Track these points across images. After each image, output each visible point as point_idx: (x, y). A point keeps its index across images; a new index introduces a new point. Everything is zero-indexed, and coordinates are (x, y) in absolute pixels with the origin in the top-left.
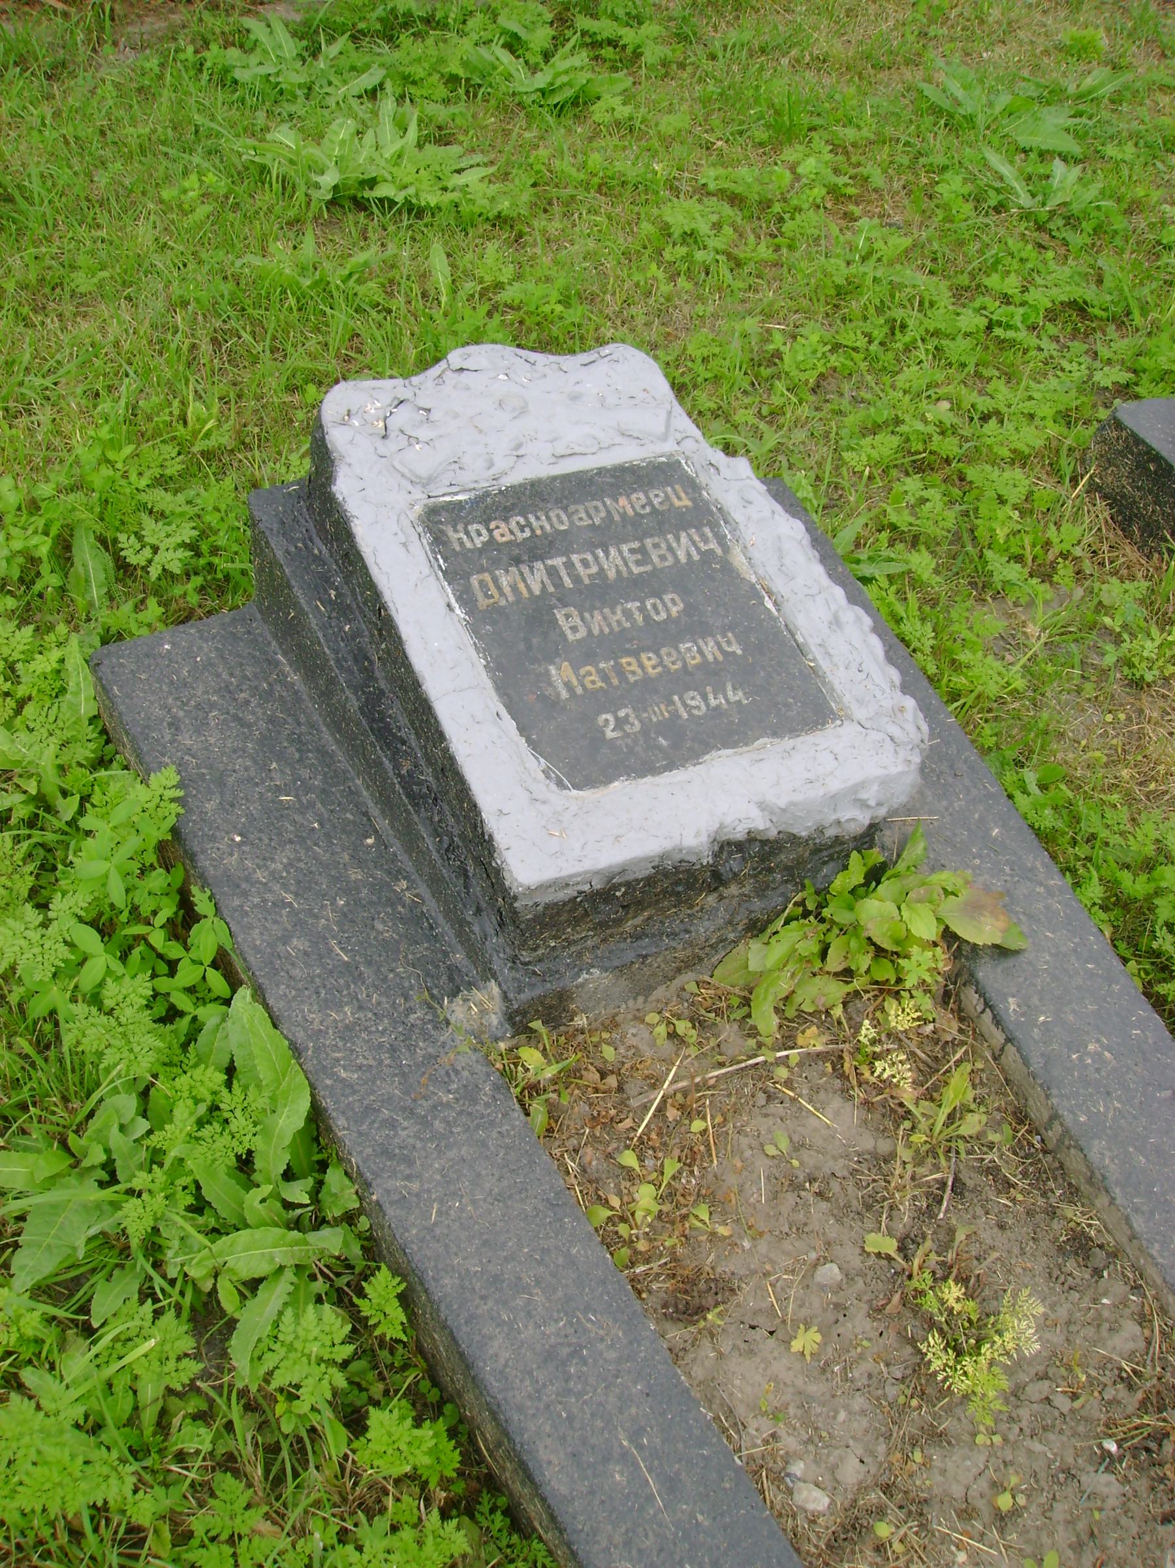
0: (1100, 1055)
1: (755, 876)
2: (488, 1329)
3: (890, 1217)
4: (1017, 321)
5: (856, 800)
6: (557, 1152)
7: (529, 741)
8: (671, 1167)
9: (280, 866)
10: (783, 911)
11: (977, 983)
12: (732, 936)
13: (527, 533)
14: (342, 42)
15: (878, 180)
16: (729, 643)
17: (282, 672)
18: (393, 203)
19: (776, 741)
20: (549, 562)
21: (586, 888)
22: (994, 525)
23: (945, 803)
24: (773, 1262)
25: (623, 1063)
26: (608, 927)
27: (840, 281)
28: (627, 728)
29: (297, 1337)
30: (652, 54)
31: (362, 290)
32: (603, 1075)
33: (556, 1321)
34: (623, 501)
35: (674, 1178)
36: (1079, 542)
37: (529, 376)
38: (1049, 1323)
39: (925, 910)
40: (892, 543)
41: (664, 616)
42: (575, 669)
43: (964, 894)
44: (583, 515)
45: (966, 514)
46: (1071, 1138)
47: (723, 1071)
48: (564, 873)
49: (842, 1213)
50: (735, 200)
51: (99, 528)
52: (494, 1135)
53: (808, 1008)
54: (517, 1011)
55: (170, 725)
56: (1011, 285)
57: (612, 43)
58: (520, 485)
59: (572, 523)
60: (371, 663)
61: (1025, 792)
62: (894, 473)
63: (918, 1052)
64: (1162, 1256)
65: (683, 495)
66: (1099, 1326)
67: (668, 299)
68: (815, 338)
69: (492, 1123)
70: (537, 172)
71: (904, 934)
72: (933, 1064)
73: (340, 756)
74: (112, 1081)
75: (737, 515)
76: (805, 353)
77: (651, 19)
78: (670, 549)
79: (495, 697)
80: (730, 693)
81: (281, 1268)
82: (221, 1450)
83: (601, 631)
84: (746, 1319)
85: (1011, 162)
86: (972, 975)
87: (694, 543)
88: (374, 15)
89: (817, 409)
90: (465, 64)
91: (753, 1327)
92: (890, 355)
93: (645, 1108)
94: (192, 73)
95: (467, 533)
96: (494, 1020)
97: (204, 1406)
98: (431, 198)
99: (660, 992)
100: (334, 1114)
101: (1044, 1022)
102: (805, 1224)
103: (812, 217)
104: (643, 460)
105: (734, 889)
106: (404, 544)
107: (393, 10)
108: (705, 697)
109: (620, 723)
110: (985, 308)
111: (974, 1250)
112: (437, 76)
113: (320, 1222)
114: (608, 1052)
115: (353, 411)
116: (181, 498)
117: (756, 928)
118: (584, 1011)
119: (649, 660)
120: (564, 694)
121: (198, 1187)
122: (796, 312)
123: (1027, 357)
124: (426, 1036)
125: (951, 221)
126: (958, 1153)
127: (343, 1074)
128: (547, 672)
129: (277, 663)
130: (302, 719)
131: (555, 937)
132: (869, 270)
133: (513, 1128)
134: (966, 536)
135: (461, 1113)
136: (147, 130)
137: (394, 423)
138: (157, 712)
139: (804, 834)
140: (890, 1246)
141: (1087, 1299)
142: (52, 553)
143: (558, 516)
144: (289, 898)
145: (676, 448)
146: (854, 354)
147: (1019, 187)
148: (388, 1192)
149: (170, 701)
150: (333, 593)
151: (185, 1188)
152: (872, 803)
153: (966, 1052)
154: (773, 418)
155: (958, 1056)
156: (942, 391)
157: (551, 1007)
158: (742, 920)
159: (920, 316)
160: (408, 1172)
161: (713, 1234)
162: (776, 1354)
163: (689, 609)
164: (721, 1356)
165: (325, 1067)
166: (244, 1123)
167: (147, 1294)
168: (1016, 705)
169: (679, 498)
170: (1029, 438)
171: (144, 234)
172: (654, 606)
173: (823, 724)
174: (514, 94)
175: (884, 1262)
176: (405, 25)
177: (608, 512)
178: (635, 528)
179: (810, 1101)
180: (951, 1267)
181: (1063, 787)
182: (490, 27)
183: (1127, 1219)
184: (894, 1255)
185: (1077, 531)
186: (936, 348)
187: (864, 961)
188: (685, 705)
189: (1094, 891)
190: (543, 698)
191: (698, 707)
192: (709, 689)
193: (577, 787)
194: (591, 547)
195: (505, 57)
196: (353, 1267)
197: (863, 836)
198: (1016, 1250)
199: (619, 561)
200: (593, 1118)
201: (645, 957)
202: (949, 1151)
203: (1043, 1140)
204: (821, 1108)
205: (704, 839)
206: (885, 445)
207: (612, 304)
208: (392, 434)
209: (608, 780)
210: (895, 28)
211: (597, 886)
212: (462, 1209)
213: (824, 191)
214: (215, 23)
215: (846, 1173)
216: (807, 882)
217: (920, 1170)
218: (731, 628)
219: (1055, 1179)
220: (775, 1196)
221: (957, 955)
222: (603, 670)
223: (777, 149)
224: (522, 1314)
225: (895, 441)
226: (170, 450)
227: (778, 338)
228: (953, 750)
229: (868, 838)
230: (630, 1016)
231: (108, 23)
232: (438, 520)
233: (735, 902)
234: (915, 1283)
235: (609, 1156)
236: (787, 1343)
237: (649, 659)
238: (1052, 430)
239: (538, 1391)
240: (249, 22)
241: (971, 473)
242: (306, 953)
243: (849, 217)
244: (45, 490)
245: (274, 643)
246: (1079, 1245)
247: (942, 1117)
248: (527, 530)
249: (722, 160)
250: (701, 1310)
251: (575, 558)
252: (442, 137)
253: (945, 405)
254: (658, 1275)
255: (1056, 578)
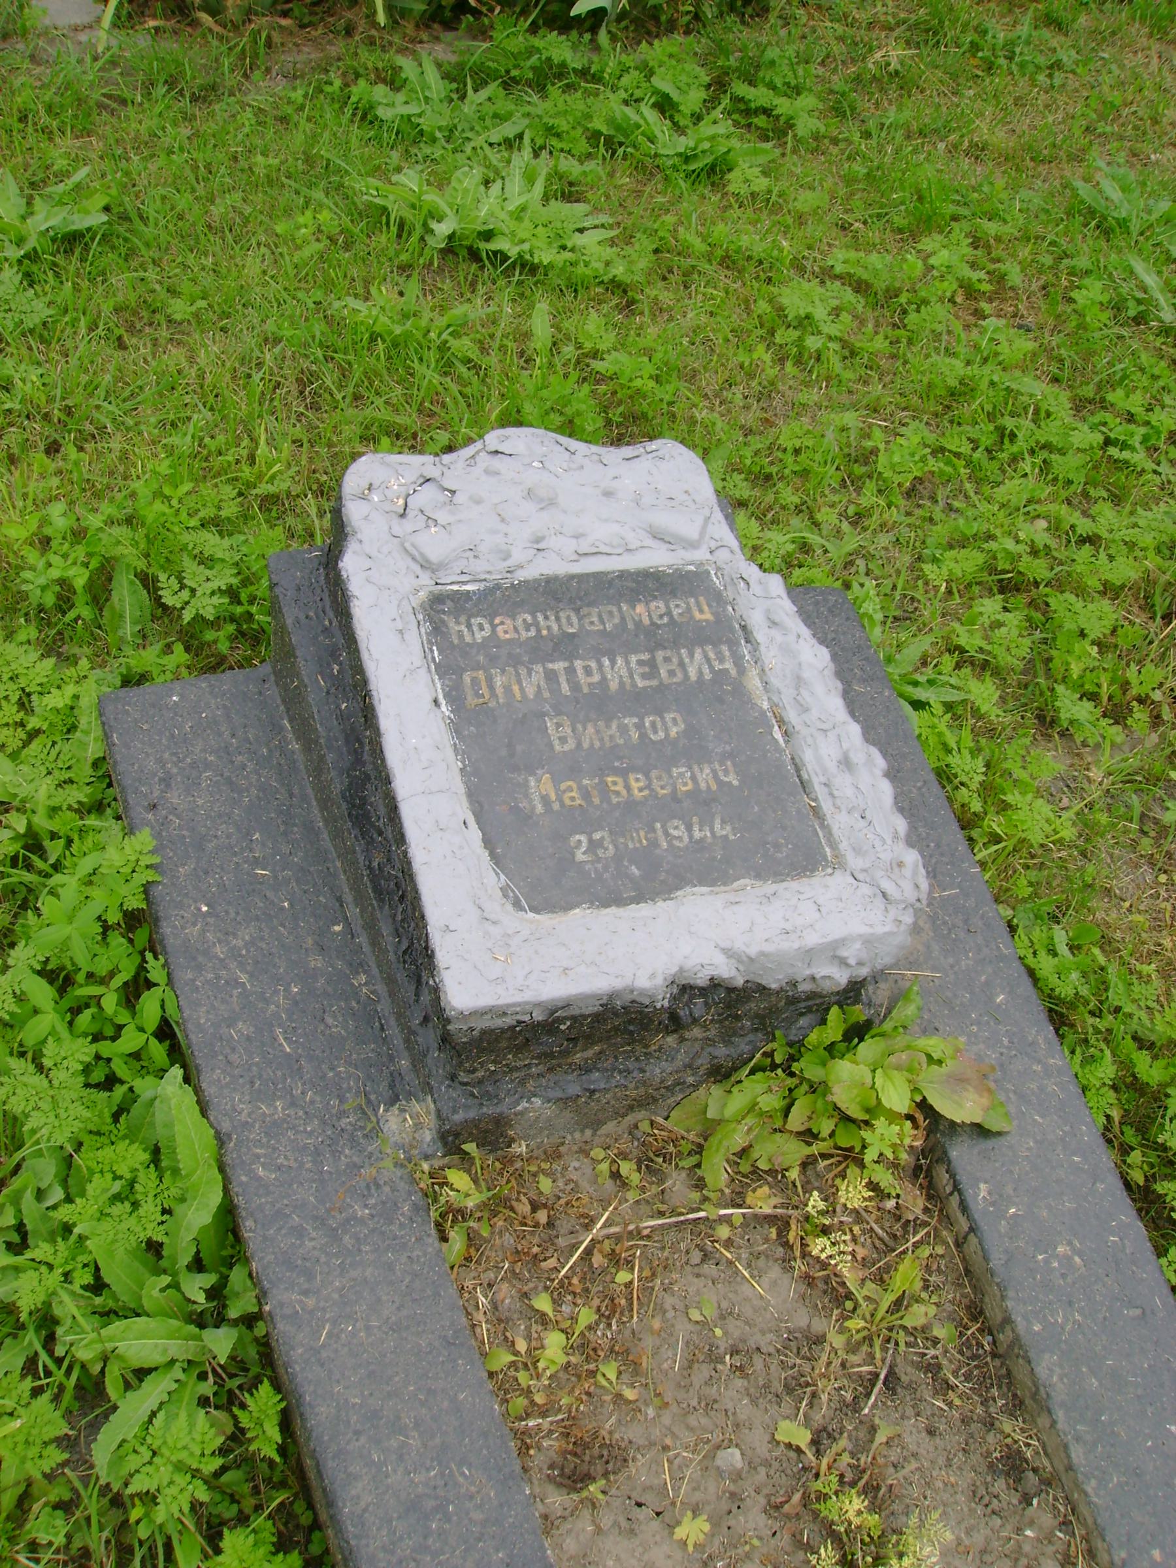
0: (1069, 1259)
1: (721, 1022)
2: (354, 1469)
3: (811, 1405)
4: (1136, 441)
5: (835, 957)
6: (469, 1283)
7: (493, 856)
8: (586, 1316)
9: (240, 943)
10: (751, 1059)
11: (949, 1162)
12: (690, 1080)
13: (532, 633)
14: (493, 88)
15: (1015, 276)
16: (726, 773)
17: (285, 737)
18: (505, 258)
19: (759, 883)
20: (550, 666)
21: (527, 1018)
22: (1069, 659)
23: (951, 960)
24: (674, 1436)
25: (559, 1198)
26: (554, 1058)
27: (953, 383)
28: (600, 852)
29: (165, 1443)
30: (806, 125)
31: (454, 343)
32: (535, 1207)
33: (428, 1470)
34: (640, 608)
35: (590, 1328)
36: (1161, 685)
37: (565, 466)
38: (961, 1549)
39: (899, 1078)
40: (958, 666)
41: (661, 735)
42: (556, 782)
43: (950, 1066)
44: (595, 619)
45: (1045, 641)
46: (1021, 1347)
47: (660, 1222)
48: (500, 1002)
49: (762, 1393)
50: (861, 287)
51: (141, 565)
52: (404, 1259)
53: (763, 1165)
54: (448, 1131)
55: (162, 780)
56: (1136, 403)
57: (766, 112)
58: (535, 580)
59: (582, 627)
60: (361, 744)
61: (1053, 952)
62: (976, 589)
63: (875, 1227)
64: (1097, 1495)
65: (706, 608)
66: (1017, 1560)
67: (772, 384)
68: (916, 440)
69: (404, 1246)
70: (661, 239)
71: (873, 1102)
72: (891, 1243)
73: (325, 836)
74: (37, 1142)
75: (761, 634)
76: (904, 453)
77: (810, 90)
78: (682, 664)
79: (465, 804)
80: (717, 826)
81: (172, 1362)
82: (77, 1544)
83: (592, 745)
84: (634, 1495)
85: (1159, 273)
86: (945, 1153)
87: (708, 660)
88: (529, 63)
89: (908, 514)
90: (611, 121)
91: (639, 1505)
92: (995, 465)
93: (574, 1247)
94: (337, 106)
95: (469, 626)
96: (428, 1136)
97: (67, 1496)
98: (545, 256)
99: (610, 1127)
100: (244, 1214)
101: (1014, 1215)
102: (715, 1401)
103: (940, 311)
104: (669, 567)
105: (696, 1032)
106: (401, 632)
107: (549, 59)
108: (689, 828)
109: (594, 845)
110: (1105, 424)
111: (894, 1455)
112: (580, 131)
113: (220, 1320)
114: (545, 1184)
115: (376, 484)
116: (226, 542)
117: (721, 1074)
118: (525, 1138)
119: (637, 783)
120: (539, 809)
121: (97, 1269)
122: (904, 409)
123: (1142, 480)
124: (353, 1143)
125: (1085, 329)
126: (897, 1344)
127: (261, 1172)
128: (526, 784)
129: (282, 729)
130: (296, 790)
131: (494, 1062)
132: (990, 372)
133: (425, 1255)
134: (1039, 666)
135: (373, 1231)
136: (277, 161)
137: (415, 502)
138: (151, 764)
139: (774, 986)
140: (802, 1438)
141: (1009, 1527)
142: (90, 586)
143: (568, 618)
144: (244, 978)
145: (708, 556)
146: (955, 460)
147: (1162, 299)
148: (282, 1305)
149: (166, 755)
150: (336, 668)
151: (85, 1265)
152: (852, 961)
153: (928, 1234)
154: (857, 520)
155: (917, 1238)
156: (1041, 509)
157: (486, 1131)
158: (703, 1062)
159: (1032, 426)
160: (306, 1286)
161: (619, 1396)
162: (658, 1538)
163: (691, 731)
164: (599, 1531)
165: (243, 1162)
166: (152, 1209)
167: (30, 1367)
168: (1063, 854)
169: (701, 611)
170: (1124, 571)
171: (253, 265)
172: (653, 724)
173: (812, 871)
174: (656, 155)
175: (793, 1454)
176: (560, 76)
177: (623, 619)
178: (652, 638)
179: (748, 1266)
180: (864, 1471)
181: (1096, 951)
182: (644, 85)
183: (1066, 1446)
184: (803, 1447)
185: (1159, 674)
186: (1044, 461)
187: (825, 1126)
188: (667, 834)
189: (1107, 1070)
190: (515, 810)
191: (680, 838)
192: (695, 819)
193: (535, 910)
194: (598, 653)
195: (651, 115)
196: (247, 1370)
197: (846, 991)
198: (941, 1461)
199: (624, 672)
200: (517, 1252)
201: (593, 1092)
202: (888, 1341)
203: (994, 1342)
204: (758, 1276)
205: (659, 981)
206: (967, 562)
207: (710, 381)
208: (411, 513)
209: (568, 907)
210: (1063, 122)
211: (538, 1016)
212: (353, 1334)
213: (955, 286)
214: (369, 59)
215: (772, 1350)
216: (778, 1033)
217: (855, 1359)
218: (731, 756)
219: (1000, 1387)
220: (690, 1364)
221: (930, 1131)
222: (586, 787)
223: (914, 236)
224: (394, 1457)
225: (980, 558)
226: (229, 491)
227: (878, 434)
228: (971, 903)
229: (853, 992)
230: (575, 1148)
231: (262, 51)
232: (441, 609)
233: (697, 1046)
234: (818, 1485)
235: (526, 1295)
236: (671, 1527)
237: (637, 780)
238: (1152, 562)
239: (393, 1543)
240: (401, 61)
241: (1056, 602)
242: (248, 1038)
243: (979, 314)
244: (94, 521)
245: (282, 708)
246: (1013, 1465)
247: (888, 1299)
248: (533, 629)
249: (856, 243)
250: (588, 1478)
251: (578, 664)
252: (570, 192)
253: (1042, 524)
254: (551, 1432)
255: (1129, 722)
